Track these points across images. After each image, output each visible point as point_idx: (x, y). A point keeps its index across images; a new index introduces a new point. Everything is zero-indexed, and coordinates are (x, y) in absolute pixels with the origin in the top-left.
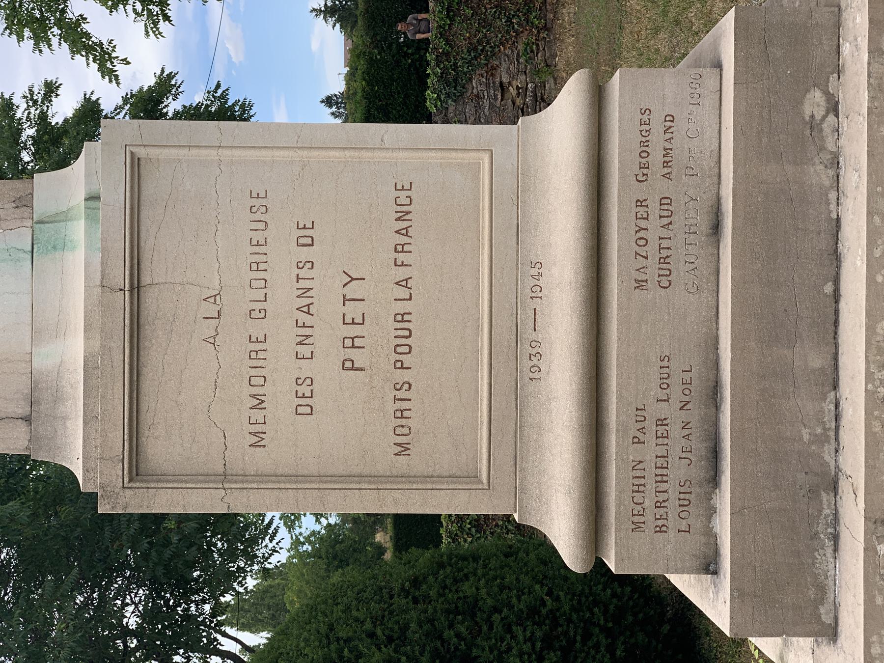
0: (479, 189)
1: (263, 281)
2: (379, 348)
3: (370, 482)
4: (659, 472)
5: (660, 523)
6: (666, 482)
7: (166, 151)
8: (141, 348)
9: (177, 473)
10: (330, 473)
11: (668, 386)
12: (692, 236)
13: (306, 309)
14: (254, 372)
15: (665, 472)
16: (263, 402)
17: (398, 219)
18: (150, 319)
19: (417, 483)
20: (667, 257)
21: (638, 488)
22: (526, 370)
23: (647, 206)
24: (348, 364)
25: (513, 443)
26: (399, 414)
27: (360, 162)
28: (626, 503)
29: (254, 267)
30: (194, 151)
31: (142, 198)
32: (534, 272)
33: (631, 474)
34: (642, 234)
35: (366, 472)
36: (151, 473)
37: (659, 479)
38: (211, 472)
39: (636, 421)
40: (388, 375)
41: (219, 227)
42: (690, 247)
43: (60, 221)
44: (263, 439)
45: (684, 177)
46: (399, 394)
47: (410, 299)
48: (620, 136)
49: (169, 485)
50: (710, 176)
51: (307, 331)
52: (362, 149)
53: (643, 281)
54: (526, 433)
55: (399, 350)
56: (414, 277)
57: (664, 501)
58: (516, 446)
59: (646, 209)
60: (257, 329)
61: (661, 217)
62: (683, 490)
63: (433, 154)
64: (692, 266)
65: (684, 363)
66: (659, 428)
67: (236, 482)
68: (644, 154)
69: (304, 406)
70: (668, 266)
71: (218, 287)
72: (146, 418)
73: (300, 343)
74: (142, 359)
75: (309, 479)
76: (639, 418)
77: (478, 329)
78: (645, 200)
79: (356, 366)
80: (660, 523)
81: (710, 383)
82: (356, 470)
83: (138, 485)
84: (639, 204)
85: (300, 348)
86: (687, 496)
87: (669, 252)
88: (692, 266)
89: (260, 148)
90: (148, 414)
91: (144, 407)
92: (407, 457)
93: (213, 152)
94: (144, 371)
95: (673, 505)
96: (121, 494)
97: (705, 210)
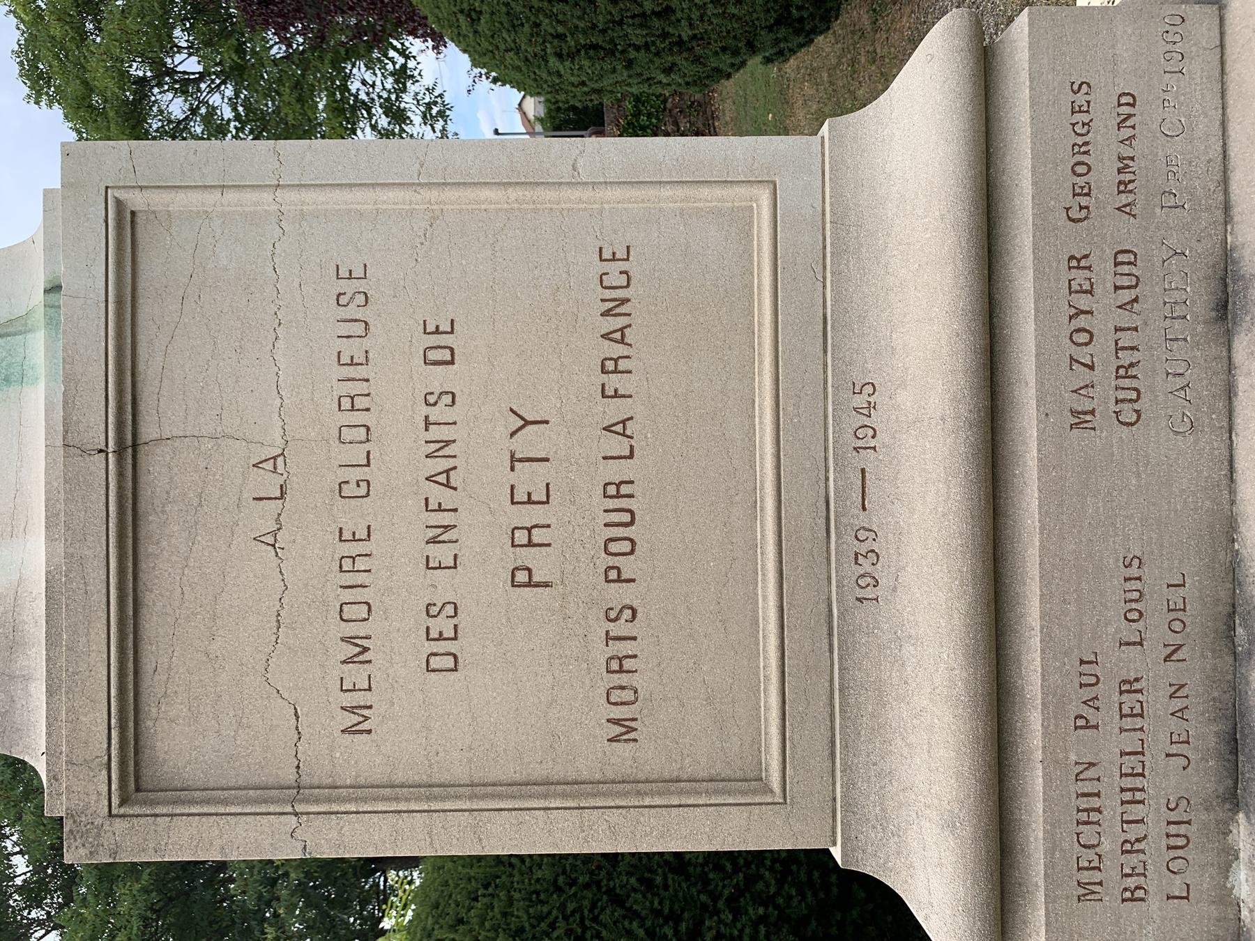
0: (751, 256)
1: (363, 430)
2: (577, 545)
3: (564, 796)
4: (1128, 782)
5: (1131, 882)
6: (1142, 802)
7: (181, 196)
8: (142, 557)
9: (211, 785)
10: (491, 778)
11: (1141, 614)
12: (1177, 324)
13: (442, 478)
14: (348, 596)
15: (1138, 782)
16: (366, 649)
17: (606, 314)
18: (157, 502)
19: (652, 794)
20: (1131, 365)
21: (1089, 816)
22: (849, 582)
23: (1089, 268)
24: (522, 577)
25: (827, 716)
26: (615, 665)
27: (535, 211)
28: (1066, 845)
29: (346, 403)
30: (231, 196)
31: (141, 284)
32: (860, 401)
33: (1073, 788)
34: (1082, 321)
35: (558, 773)
36: (163, 784)
37: (1128, 796)
38: (272, 781)
39: (1081, 685)
40: (595, 593)
41: (280, 331)
42: (1175, 345)
43: (15, 334)
44: (366, 718)
45: (1158, 210)
46: (618, 629)
47: (631, 456)
48: (1034, 135)
49: (193, 810)
50: (1208, 209)
51: (446, 518)
52: (538, 184)
53: (1085, 413)
54: (852, 701)
55: (613, 547)
56: (637, 417)
57: (1138, 840)
58: (832, 721)
59: (1087, 273)
60: (352, 517)
61: (1117, 288)
62: (1174, 816)
63: (666, 192)
64: (1180, 382)
65: (1171, 569)
66: (1125, 697)
67: (317, 801)
68: (1081, 168)
69: (443, 652)
70: (1134, 383)
71: (279, 442)
72: (153, 685)
73: (433, 541)
74: (143, 576)
75: (451, 790)
76: (1085, 680)
77: (754, 508)
78: (1086, 256)
79: (536, 579)
80: (1131, 882)
81: (1220, 608)
82: (539, 772)
83: (137, 810)
84: (1074, 263)
85: (433, 550)
86: (1182, 829)
87: (1136, 356)
88: (1180, 382)
89: (351, 186)
90: (157, 677)
91: (147, 665)
92: (632, 744)
93: (267, 196)
94: (148, 598)
95: (1155, 847)
96: (106, 827)
97: (1201, 274)
